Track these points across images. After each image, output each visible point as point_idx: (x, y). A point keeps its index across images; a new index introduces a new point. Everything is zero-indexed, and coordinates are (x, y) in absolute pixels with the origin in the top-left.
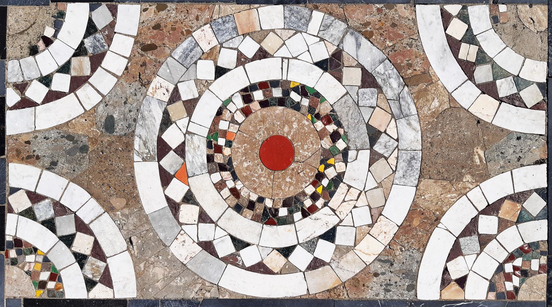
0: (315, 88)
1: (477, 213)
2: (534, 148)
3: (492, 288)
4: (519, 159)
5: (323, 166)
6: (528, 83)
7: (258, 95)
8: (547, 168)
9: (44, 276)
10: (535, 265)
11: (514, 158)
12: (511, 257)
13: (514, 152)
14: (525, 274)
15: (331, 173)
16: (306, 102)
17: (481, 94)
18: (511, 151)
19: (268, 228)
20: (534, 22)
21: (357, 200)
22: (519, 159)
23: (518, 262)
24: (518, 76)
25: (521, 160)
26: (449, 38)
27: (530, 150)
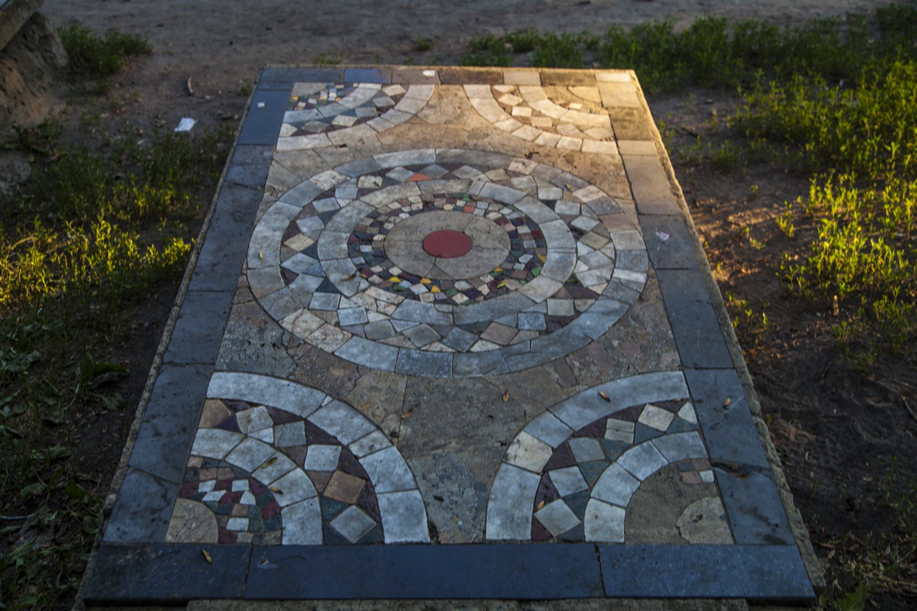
0: (555, 447)
1: (345, 442)
2: (460, 523)
3: (207, 463)
4: (440, 499)
5: (429, 282)
6: (579, 511)
7: (523, 230)
8: (422, 543)
9: (312, 101)
10: (237, 524)
11: (441, 490)
12: (256, 487)
13: (452, 493)
14: (224, 508)
15: (419, 289)
16: (520, 267)
17: (553, 449)
18: (455, 489)
19: (437, 525)
20: (696, 521)
21: (377, 311)
22: (440, 499)
23: (248, 499)
24: (581, 150)
25: (437, 503)
26: (640, 409)
27: (457, 516)
